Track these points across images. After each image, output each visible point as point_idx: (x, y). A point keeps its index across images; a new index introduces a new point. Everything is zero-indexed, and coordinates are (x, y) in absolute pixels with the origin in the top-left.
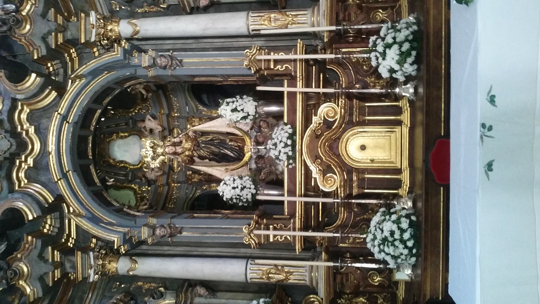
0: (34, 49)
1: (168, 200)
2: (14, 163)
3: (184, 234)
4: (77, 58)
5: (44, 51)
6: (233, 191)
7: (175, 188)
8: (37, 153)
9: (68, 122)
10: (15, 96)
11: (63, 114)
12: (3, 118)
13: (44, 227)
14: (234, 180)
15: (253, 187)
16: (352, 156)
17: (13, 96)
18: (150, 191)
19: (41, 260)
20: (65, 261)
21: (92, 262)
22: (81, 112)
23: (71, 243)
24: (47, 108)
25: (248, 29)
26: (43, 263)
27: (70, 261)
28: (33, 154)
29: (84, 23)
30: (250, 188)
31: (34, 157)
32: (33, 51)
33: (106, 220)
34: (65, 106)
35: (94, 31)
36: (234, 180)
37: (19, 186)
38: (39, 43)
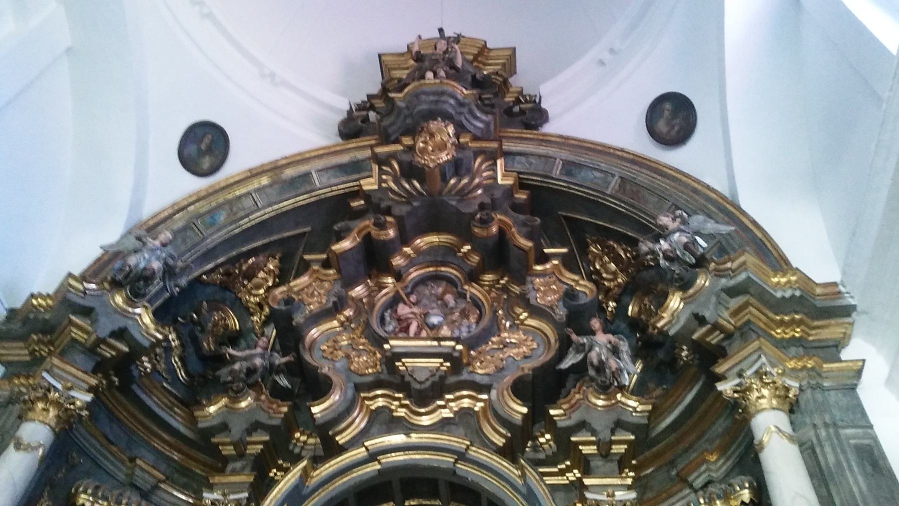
4: (567, 482)
5: (562, 423)
8: (412, 421)
9: (456, 461)
10: (495, 389)
11: (469, 454)
12: (462, 375)
13: (302, 434)
19: (252, 425)
21: (232, 497)
22: (472, 480)
23: (276, 474)
26: (246, 427)
27: (243, 468)
28: (412, 416)
29: (615, 483)
32: (561, 408)
34: (480, 456)
38: (576, 417)
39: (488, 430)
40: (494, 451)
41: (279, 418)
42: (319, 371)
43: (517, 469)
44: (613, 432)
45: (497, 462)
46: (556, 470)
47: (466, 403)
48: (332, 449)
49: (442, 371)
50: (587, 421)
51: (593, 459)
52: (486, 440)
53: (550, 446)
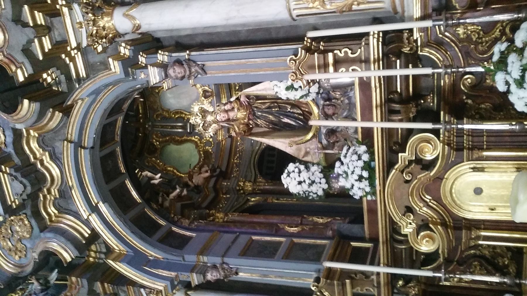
0: (17, 68)
1: (233, 154)
2: (38, 197)
3: (241, 274)
6: (299, 187)
7: (235, 165)
8: (60, 183)
9: (84, 148)
14: (300, 172)
15: (324, 181)
16: (458, 199)
17: (12, 126)
18: (212, 143)
20: (118, 291)
24: (57, 130)
25: (291, 15)
29: (70, 21)
30: (320, 183)
31: (58, 187)
33: (152, 256)
34: (74, 131)
35: (84, 30)
36: (300, 172)
37: (51, 221)
38: (20, 57)
39: (53, 124)
40: (68, 117)
41: (81, 281)
42: (38, 261)
43: (77, 103)
44: (25, 25)
45: (76, 117)
46: (71, 64)
47: (34, 145)
48: (95, 236)
49: (10, 171)
50: (21, 48)
51: (54, 39)
52: (61, 125)
53: (53, 72)
